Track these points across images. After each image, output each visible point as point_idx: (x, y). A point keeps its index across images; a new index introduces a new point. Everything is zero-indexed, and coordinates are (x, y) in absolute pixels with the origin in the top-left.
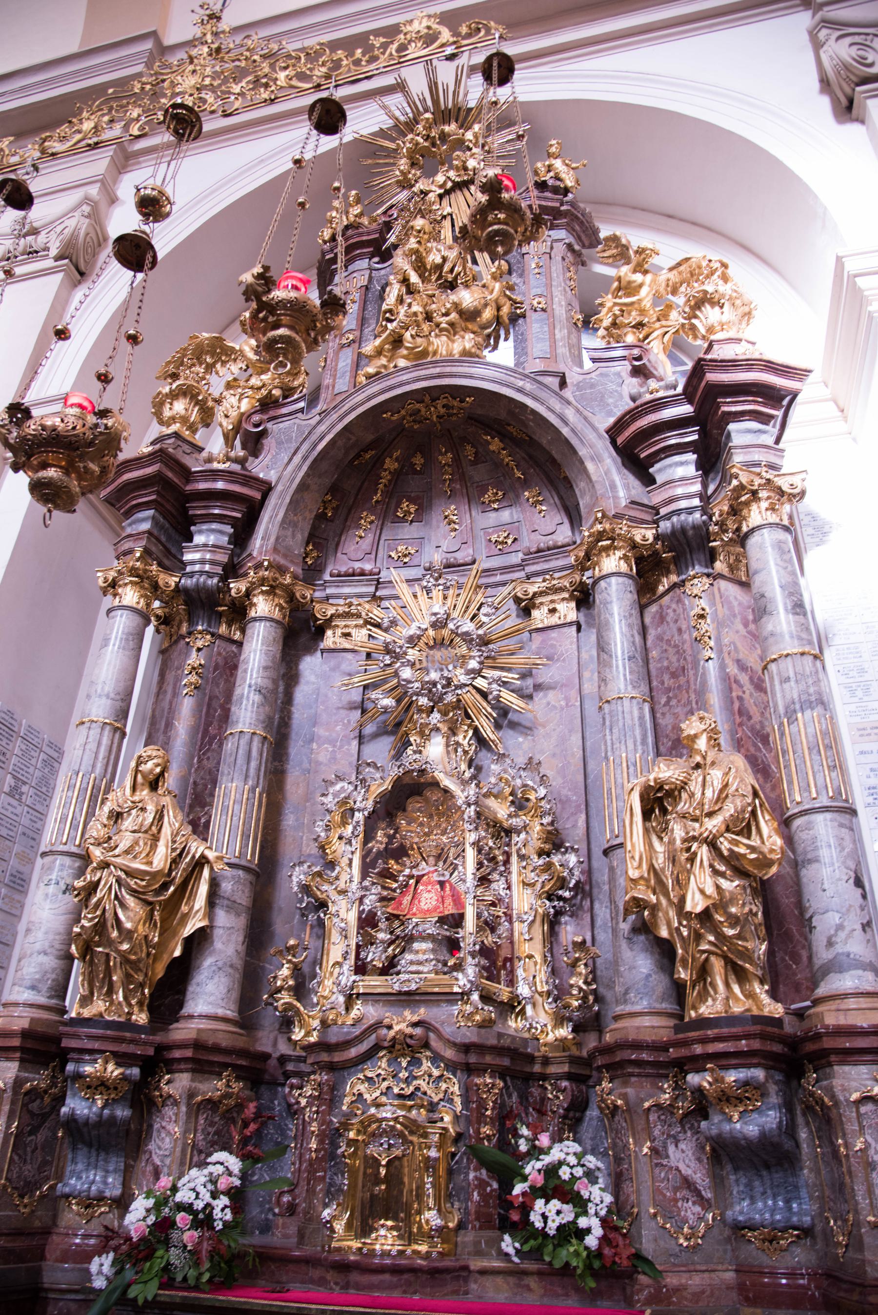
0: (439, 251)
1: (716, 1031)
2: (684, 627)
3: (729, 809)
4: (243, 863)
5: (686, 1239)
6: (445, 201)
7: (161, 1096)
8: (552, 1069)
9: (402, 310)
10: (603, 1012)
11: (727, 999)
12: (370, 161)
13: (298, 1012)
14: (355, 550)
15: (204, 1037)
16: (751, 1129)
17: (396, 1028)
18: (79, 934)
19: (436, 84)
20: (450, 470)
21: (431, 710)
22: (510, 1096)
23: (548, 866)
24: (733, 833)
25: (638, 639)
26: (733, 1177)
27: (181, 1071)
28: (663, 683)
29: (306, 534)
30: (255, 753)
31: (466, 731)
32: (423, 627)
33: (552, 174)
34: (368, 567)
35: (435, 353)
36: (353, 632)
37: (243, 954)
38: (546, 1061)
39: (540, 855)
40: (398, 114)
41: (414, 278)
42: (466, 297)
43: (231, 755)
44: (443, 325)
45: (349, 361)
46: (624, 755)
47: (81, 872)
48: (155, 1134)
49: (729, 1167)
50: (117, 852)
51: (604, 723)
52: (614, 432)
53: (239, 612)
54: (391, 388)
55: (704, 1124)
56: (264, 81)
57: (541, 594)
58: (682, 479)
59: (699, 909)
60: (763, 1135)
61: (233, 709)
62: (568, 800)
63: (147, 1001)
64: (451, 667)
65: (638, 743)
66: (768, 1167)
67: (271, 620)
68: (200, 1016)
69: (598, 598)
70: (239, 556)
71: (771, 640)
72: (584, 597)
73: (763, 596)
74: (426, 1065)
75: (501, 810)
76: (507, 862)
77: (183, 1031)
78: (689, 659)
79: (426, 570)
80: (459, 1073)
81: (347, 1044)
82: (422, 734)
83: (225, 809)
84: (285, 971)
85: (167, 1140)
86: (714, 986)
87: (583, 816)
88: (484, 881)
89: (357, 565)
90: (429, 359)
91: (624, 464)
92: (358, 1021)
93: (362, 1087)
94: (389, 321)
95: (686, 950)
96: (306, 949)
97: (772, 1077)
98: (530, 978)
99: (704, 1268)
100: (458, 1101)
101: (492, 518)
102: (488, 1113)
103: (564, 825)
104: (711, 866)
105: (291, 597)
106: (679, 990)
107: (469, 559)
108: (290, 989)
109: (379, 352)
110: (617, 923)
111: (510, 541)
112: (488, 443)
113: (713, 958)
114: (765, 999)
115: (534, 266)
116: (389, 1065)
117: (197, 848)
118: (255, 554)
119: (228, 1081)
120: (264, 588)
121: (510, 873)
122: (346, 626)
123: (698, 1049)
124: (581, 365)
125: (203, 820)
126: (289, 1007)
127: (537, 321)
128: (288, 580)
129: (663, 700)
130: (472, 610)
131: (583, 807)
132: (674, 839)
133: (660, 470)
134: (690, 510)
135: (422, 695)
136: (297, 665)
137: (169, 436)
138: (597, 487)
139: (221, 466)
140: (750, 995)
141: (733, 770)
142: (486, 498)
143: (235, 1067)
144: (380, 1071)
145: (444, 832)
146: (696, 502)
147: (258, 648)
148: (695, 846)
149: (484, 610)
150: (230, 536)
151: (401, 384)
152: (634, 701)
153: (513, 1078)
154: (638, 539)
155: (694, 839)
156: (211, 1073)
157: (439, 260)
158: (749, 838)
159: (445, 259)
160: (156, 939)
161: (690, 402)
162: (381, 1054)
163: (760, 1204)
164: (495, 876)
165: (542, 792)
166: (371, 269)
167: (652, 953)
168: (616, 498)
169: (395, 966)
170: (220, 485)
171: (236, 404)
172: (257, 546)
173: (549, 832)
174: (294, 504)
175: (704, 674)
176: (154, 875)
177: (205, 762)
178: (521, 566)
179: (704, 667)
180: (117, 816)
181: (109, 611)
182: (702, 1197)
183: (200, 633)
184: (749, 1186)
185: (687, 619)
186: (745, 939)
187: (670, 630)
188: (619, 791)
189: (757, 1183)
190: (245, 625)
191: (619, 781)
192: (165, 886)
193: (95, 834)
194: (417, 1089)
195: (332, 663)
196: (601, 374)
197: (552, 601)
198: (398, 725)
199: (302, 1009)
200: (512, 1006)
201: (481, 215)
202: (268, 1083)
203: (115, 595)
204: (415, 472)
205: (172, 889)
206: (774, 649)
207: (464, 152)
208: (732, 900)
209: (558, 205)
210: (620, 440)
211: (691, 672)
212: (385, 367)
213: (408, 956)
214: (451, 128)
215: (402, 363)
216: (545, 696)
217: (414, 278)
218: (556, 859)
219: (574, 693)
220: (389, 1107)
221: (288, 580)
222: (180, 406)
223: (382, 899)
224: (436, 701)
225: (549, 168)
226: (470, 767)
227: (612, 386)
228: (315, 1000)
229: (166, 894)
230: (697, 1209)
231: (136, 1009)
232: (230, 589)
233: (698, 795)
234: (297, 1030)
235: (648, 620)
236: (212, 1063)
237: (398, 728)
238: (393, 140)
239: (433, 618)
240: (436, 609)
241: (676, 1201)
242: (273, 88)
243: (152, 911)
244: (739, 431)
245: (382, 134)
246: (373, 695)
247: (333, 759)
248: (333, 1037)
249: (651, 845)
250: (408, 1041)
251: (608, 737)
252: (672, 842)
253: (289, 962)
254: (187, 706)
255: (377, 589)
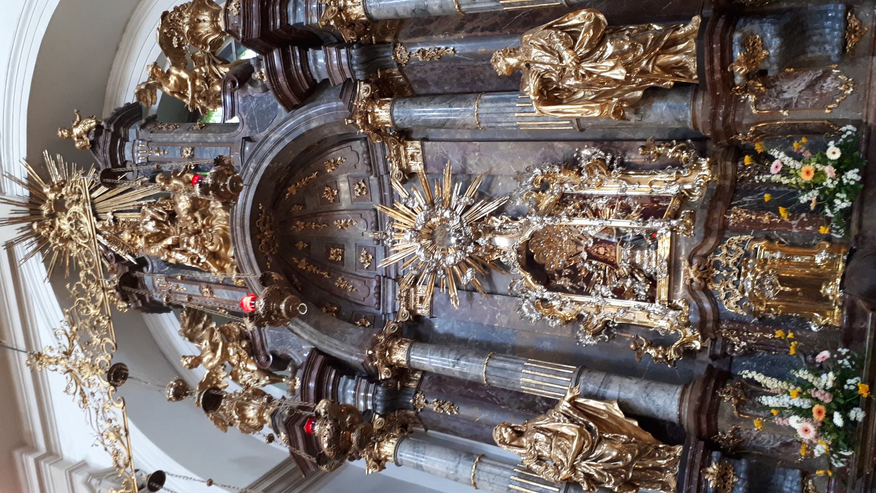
0: (146, 223)
1: (706, 64)
2: (430, 66)
3: (559, 46)
4: (575, 376)
5: (848, 89)
6: (102, 216)
7: (733, 439)
8: (730, 172)
9: (192, 250)
10: (694, 136)
11: (686, 54)
12: (67, 271)
13: (682, 344)
14: (360, 291)
15: (693, 408)
16: (776, 42)
17: (692, 276)
18: (619, 487)
19: (11, 219)
20: (309, 224)
21: (477, 244)
22: (745, 202)
23: (590, 171)
24: (575, 44)
25: (437, 99)
26: (809, 55)
27: (716, 424)
28: (468, 84)
29: (350, 325)
30: (501, 364)
31: (492, 221)
32: (419, 246)
33: (84, 136)
34: (375, 283)
35: (224, 229)
36: (419, 295)
37: (639, 380)
38: (724, 177)
39: (581, 175)
40: (31, 249)
41: (169, 241)
42: (183, 204)
43: (501, 381)
44: (204, 222)
45: (224, 291)
46: (516, 115)
47: (577, 485)
48: (759, 445)
49: (802, 57)
50: (564, 460)
51: (494, 127)
52: (290, 107)
53: (402, 373)
54: (250, 261)
55: (770, 74)
56: (95, 323)
57: (400, 165)
58: (326, 59)
59: (624, 71)
60: (779, 34)
61: (469, 378)
62: (544, 153)
63: (668, 446)
64: (448, 230)
65: (509, 104)
66: (804, 32)
67: (409, 350)
68: (680, 410)
69: (407, 125)
70: (362, 373)
71: (445, 8)
72: (404, 134)
73: (414, 11)
74: (719, 257)
75: (547, 199)
76: (584, 197)
77: (689, 422)
78: (452, 64)
79: (378, 244)
80: (727, 236)
81: (702, 311)
82: (492, 251)
83: (538, 386)
84: (652, 352)
85: (763, 436)
86: (677, 62)
87: (556, 143)
88: (596, 213)
89: (373, 291)
90: (229, 234)
91: (312, 101)
92: (687, 303)
93: (732, 301)
94: (199, 259)
95: (652, 81)
96: (637, 337)
97: (741, 27)
98: (663, 185)
99: (868, 79)
100: (744, 237)
101: (345, 196)
102: (754, 217)
103: (560, 157)
104: (596, 61)
105: (394, 337)
106: (680, 87)
107: (373, 214)
108: (665, 349)
109: (222, 269)
110: (631, 124)
111: (363, 185)
112: (291, 194)
113: (658, 62)
114: (689, 27)
115: (158, 154)
116: (718, 283)
117: (565, 405)
118: (362, 360)
119: (725, 393)
120: (387, 354)
121: (592, 195)
122: (415, 300)
123: (718, 76)
124: (237, 125)
125: (545, 404)
126: (677, 350)
127: (201, 154)
128: (382, 338)
129: (480, 84)
130: (409, 211)
131: (549, 143)
132: (576, 84)
133: (319, 75)
134: (349, 57)
135: (466, 249)
136: (439, 335)
137: (273, 421)
138: (328, 121)
139: (298, 383)
140: (685, 38)
141: (532, 41)
142: (331, 199)
143: (716, 387)
144: (722, 289)
145: (561, 239)
146: (343, 52)
147: (430, 360)
148: (581, 71)
149: (410, 205)
150: (348, 378)
151: (247, 254)
152: (480, 105)
153: (732, 200)
154: (366, 95)
155: (576, 72)
156: (718, 405)
157: (153, 223)
158: (579, 33)
159: (153, 219)
160: (625, 437)
161: (271, 51)
162: (710, 287)
163: (829, 37)
164: (593, 206)
165: (537, 171)
166: (152, 272)
167: (653, 102)
168: (337, 109)
169: (651, 276)
170: (312, 385)
171: (249, 374)
172: (356, 359)
173: (566, 167)
174: (329, 332)
175: (464, 55)
176: (582, 434)
177: (504, 401)
178: (380, 178)
179: (459, 54)
180: (540, 459)
181: (397, 464)
182: (821, 76)
183: (415, 401)
184: (816, 44)
185: (425, 63)
186: (647, 40)
187: (432, 76)
188: (541, 119)
189: (815, 38)
190: (412, 368)
191: (533, 119)
192: (589, 428)
193: (552, 475)
194: (735, 264)
195: (440, 310)
196: (244, 111)
197: (406, 157)
198: (485, 267)
199: (678, 342)
200: (683, 198)
201: (219, 196)
202: (730, 368)
203: (386, 460)
204: (309, 247)
205: (591, 424)
206: (451, 6)
207: (65, 201)
208: (620, 47)
209: (110, 134)
210: (296, 102)
211: (462, 63)
212: (232, 265)
213: (645, 267)
214: (45, 210)
215: (231, 253)
216: (471, 166)
217: (169, 241)
218: (584, 164)
219: (471, 146)
220: (745, 283)
221: (382, 338)
222: (251, 413)
223: (605, 284)
224: (469, 241)
225: (80, 137)
226: (517, 220)
227: (253, 104)
228: (673, 332)
229: (594, 428)
230: (829, 80)
231: (672, 453)
232: (386, 379)
233: (548, 67)
234: (693, 346)
235: (423, 91)
236: (711, 405)
237: (488, 267)
238: (52, 253)
239: (414, 240)
240: (407, 237)
241: (822, 95)
242: (101, 318)
243: (605, 438)
244: (295, 18)
245: (46, 261)
246: (464, 282)
247: (506, 312)
248: (694, 318)
249: (580, 100)
250: (701, 268)
251: (503, 125)
252: (577, 86)
253: (646, 348)
254: (466, 412)
255: (390, 278)
